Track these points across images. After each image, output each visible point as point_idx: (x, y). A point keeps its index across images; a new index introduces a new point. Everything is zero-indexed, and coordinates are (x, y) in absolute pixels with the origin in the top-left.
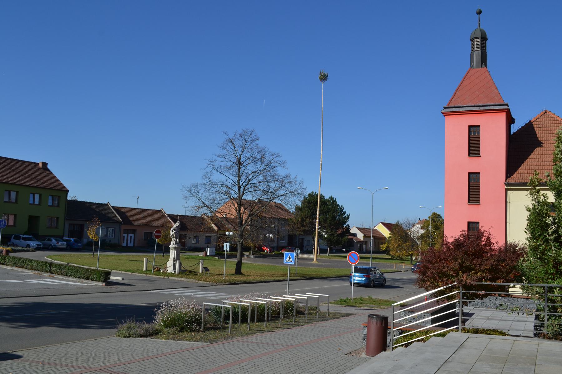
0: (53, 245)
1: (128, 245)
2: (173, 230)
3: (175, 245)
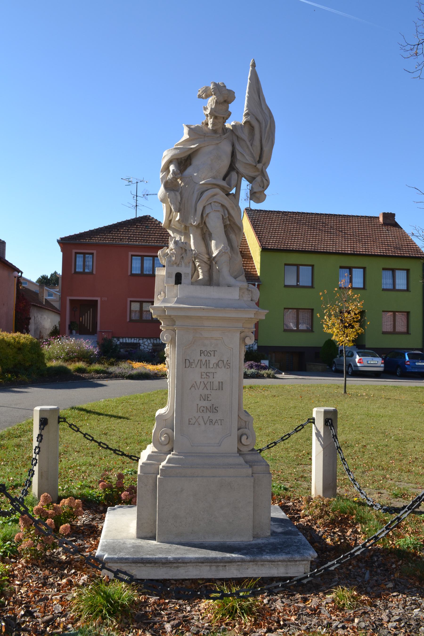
0: (352, 365)
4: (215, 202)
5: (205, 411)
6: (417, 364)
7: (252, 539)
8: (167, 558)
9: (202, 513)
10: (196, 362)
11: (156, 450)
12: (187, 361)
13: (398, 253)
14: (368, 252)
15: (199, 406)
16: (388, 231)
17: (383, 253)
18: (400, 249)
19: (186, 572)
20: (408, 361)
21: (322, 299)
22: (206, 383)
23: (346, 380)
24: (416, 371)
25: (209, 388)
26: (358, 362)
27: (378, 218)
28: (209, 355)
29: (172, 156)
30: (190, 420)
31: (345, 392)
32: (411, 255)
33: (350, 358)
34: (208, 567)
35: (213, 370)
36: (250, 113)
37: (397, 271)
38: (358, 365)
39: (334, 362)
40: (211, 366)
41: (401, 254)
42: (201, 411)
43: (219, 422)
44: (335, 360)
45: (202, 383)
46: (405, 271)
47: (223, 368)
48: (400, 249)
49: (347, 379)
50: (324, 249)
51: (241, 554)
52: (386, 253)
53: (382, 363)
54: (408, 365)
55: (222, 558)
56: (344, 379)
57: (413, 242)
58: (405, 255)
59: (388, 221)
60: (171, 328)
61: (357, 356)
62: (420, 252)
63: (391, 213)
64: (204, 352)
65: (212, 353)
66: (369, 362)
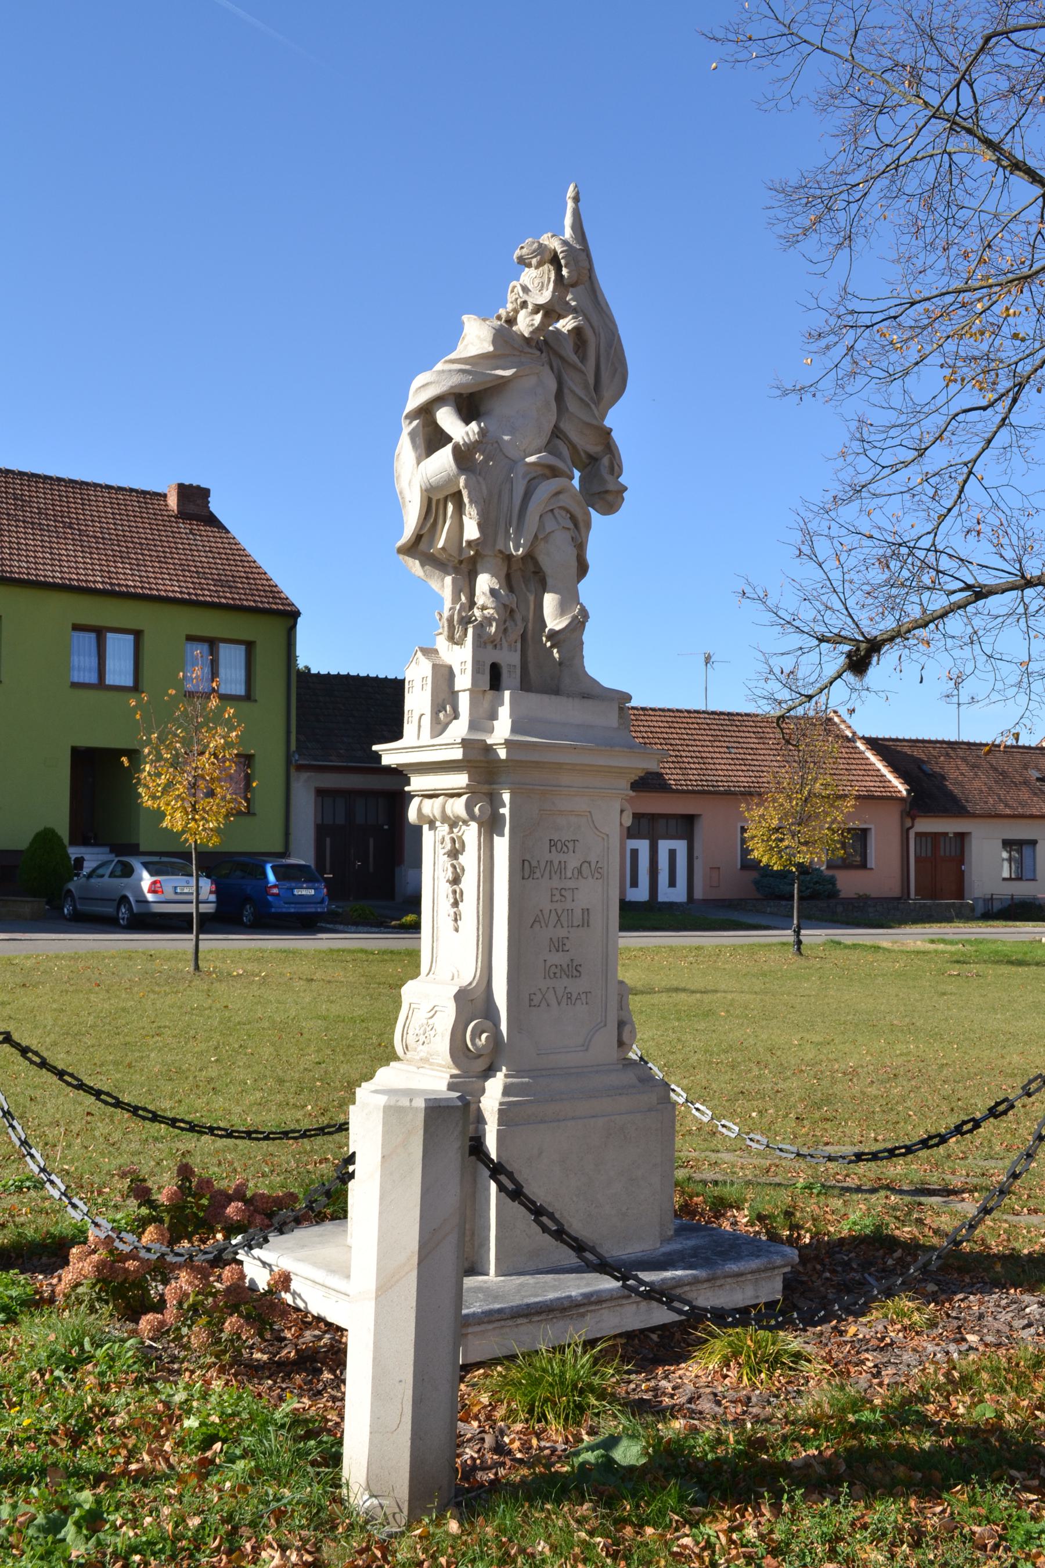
0: (131, 899)
1: (661, 898)
2: (447, 419)
3: (482, 719)
4: (560, 508)
5: (558, 975)
6: (297, 892)
7: (658, 1245)
8: (570, 1297)
9: (575, 1199)
10: (543, 864)
11: (456, 1072)
12: (526, 863)
13: (225, 598)
14: (150, 589)
15: (549, 964)
16: (193, 534)
17: (189, 594)
18: (230, 587)
19: (597, 1323)
20: (275, 886)
21: (138, 717)
22: (559, 913)
23: (197, 940)
24: (292, 910)
25: (565, 924)
26: (150, 891)
27: (165, 496)
28: (565, 848)
29: (452, 387)
30: (533, 997)
31: (197, 967)
32: (260, 605)
33: (125, 880)
34: (635, 1306)
35: (571, 884)
36: (578, 309)
37: (221, 645)
38: (150, 897)
39: (69, 891)
40: (569, 875)
41: (233, 599)
42: (552, 975)
43: (583, 996)
44: (71, 886)
45: (553, 912)
46: (243, 647)
47: (590, 878)
48: (230, 587)
49: (201, 936)
50: (29, 574)
51: (684, 1269)
52: (196, 595)
53: (211, 892)
54: (273, 895)
55: (662, 1280)
56: (193, 936)
57: (260, 571)
58: (245, 603)
59: (192, 509)
60: (485, 788)
61: (145, 875)
62: (280, 598)
63: (198, 487)
64: (555, 845)
65: (570, 845)
66: (179, 891)
